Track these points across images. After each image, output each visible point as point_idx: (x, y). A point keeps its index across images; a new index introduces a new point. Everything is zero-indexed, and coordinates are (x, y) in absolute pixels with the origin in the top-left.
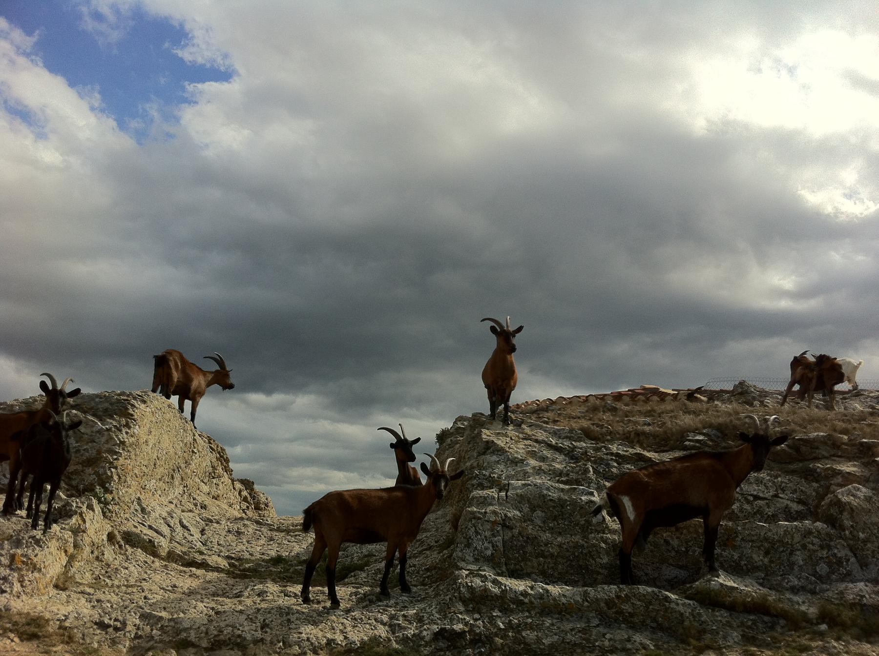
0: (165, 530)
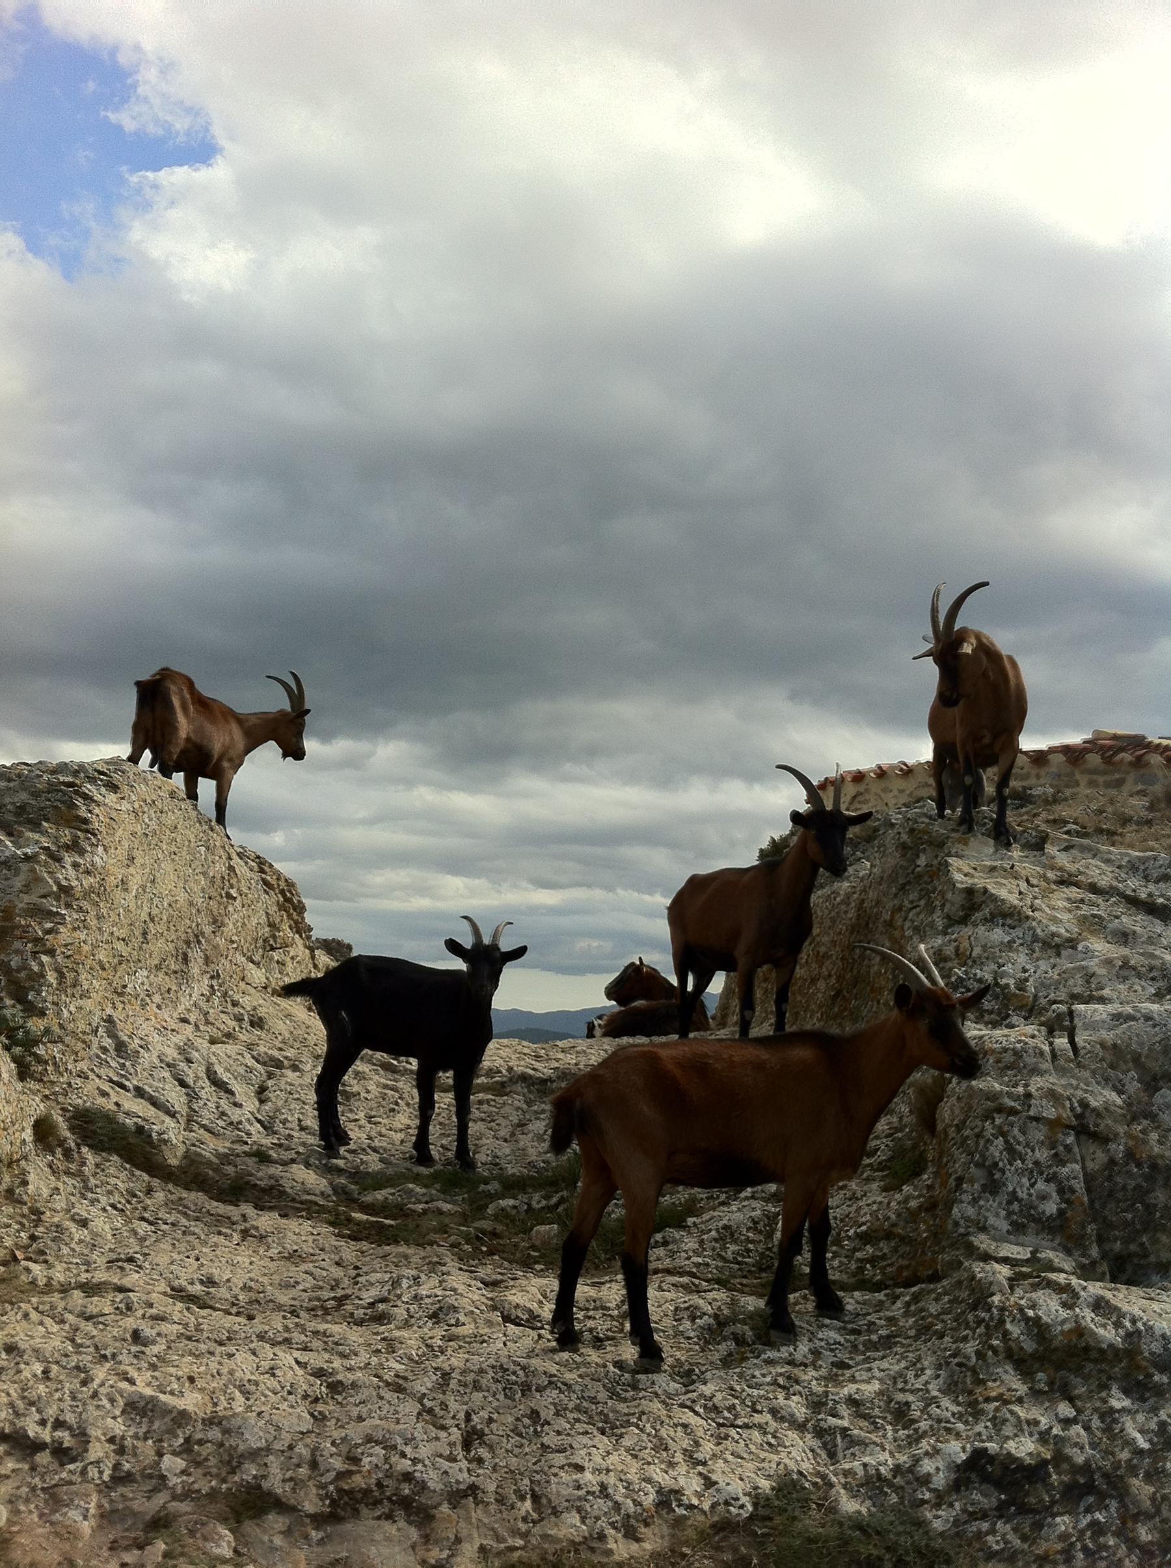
0: (175, 1097)
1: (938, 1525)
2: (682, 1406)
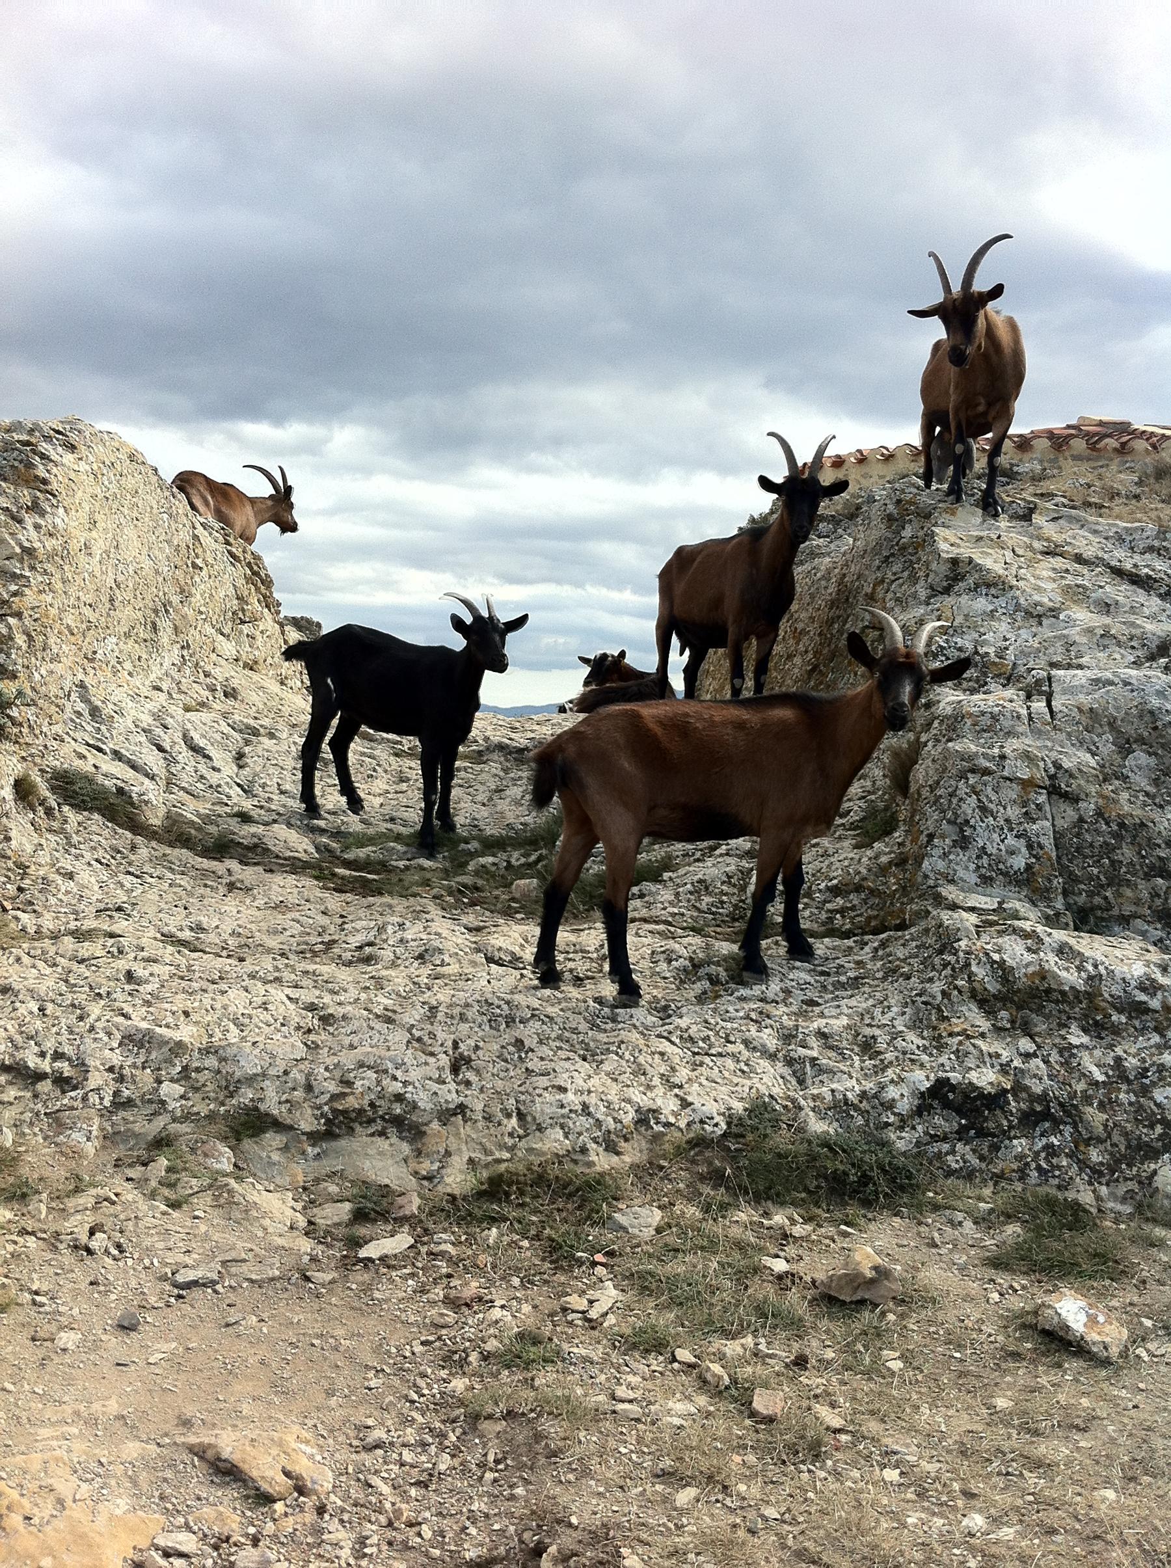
0: (153, 760)
1: (901, 1145)
2: (659, 1036)
